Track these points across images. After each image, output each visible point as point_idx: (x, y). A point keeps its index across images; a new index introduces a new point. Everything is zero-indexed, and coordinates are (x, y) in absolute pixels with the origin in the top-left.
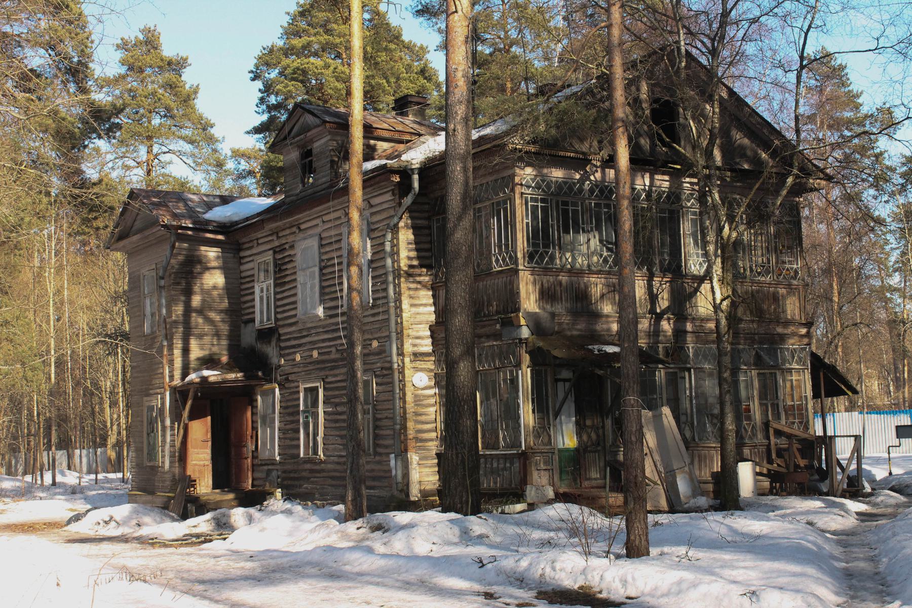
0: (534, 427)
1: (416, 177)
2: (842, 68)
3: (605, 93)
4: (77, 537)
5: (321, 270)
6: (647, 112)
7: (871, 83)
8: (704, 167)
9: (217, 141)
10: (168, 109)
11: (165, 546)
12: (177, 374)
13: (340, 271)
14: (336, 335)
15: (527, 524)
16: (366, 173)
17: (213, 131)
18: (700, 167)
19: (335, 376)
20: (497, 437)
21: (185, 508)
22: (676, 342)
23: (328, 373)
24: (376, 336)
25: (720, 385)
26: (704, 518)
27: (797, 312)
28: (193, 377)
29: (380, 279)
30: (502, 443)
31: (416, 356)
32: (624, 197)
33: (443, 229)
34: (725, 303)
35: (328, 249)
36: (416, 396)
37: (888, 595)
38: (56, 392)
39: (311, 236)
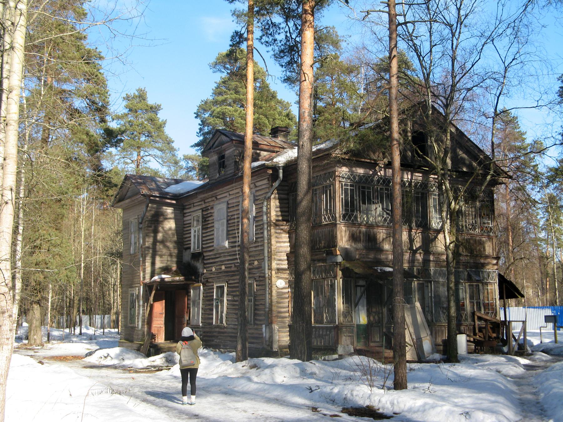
0: (343, 312)
1: (281, 171)
2: (515, 118)
3: (387, 127)
4: (89, 364)
5: (228, 221)
6: (410, 138)
7: (534, 124)
8: (441, 169)
9: (175, 150)
10: (149, 132)
11: (136, 372)
12: (148, 276)
13: (238, 222)
14: (235, 257)
15: (338, 367)
16: (254, 168)
17: (173, 145)
18: (439, 169)
19: (234, 280)
20: (323, 316)
21: (149, 350)
22: (424, 266)
23: (230, 278)
24: (257, 258)
25: (448, 291)
26: (439, 367)
27: (491, 251)
28: (156, 278)
29: (260, 228)
30: (325, 320)
31: (279, 270)
32: (396, 183)
33: (295, 200)
34: (452, 245)
35: (231, 210)
36: (278, 292)
37: (545, 416)
38: (85, 283)
39: (223, 202)
